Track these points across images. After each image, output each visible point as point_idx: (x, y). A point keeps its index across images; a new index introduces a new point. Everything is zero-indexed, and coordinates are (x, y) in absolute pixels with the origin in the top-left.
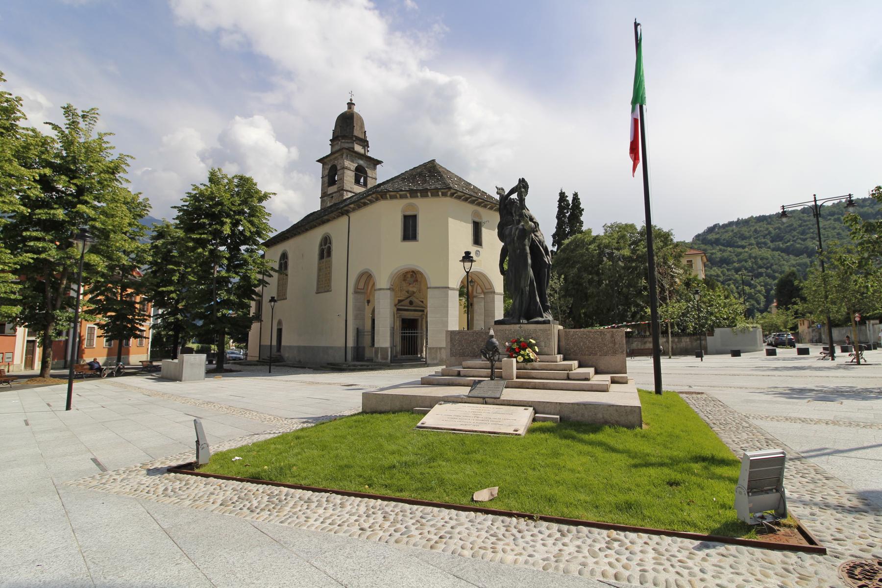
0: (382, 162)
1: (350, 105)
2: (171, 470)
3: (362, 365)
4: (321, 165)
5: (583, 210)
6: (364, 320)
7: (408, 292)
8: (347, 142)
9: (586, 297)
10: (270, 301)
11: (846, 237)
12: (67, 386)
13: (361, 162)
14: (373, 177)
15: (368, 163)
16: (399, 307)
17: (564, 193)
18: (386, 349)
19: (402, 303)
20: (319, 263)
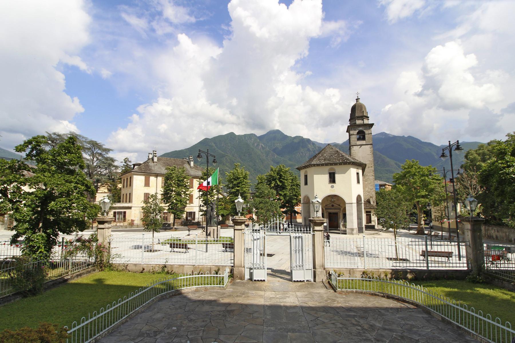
6: (352, 207)
7: (331, 201)
11: (405, 331)
13: (361, 129)
14: (369, 133)
15: (365, 127)
19: (328, 206)
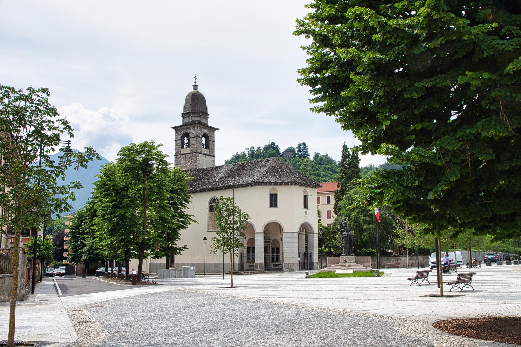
0: (218, 129)
1: (195, 87)
2: (51, 343)
3: (251, 272)
4: (174, 131)
5: (360, 160)
8: (196, 117)
9: (363, 231)
10: (204, 239)
12: (230, 277)
13: (206, 131)
16: (267, 240)
17: (346, 146)
18: (263, 263)
20: (209, 214)
